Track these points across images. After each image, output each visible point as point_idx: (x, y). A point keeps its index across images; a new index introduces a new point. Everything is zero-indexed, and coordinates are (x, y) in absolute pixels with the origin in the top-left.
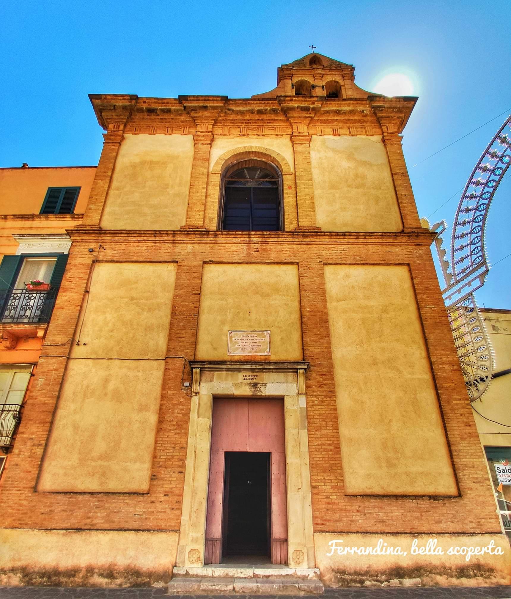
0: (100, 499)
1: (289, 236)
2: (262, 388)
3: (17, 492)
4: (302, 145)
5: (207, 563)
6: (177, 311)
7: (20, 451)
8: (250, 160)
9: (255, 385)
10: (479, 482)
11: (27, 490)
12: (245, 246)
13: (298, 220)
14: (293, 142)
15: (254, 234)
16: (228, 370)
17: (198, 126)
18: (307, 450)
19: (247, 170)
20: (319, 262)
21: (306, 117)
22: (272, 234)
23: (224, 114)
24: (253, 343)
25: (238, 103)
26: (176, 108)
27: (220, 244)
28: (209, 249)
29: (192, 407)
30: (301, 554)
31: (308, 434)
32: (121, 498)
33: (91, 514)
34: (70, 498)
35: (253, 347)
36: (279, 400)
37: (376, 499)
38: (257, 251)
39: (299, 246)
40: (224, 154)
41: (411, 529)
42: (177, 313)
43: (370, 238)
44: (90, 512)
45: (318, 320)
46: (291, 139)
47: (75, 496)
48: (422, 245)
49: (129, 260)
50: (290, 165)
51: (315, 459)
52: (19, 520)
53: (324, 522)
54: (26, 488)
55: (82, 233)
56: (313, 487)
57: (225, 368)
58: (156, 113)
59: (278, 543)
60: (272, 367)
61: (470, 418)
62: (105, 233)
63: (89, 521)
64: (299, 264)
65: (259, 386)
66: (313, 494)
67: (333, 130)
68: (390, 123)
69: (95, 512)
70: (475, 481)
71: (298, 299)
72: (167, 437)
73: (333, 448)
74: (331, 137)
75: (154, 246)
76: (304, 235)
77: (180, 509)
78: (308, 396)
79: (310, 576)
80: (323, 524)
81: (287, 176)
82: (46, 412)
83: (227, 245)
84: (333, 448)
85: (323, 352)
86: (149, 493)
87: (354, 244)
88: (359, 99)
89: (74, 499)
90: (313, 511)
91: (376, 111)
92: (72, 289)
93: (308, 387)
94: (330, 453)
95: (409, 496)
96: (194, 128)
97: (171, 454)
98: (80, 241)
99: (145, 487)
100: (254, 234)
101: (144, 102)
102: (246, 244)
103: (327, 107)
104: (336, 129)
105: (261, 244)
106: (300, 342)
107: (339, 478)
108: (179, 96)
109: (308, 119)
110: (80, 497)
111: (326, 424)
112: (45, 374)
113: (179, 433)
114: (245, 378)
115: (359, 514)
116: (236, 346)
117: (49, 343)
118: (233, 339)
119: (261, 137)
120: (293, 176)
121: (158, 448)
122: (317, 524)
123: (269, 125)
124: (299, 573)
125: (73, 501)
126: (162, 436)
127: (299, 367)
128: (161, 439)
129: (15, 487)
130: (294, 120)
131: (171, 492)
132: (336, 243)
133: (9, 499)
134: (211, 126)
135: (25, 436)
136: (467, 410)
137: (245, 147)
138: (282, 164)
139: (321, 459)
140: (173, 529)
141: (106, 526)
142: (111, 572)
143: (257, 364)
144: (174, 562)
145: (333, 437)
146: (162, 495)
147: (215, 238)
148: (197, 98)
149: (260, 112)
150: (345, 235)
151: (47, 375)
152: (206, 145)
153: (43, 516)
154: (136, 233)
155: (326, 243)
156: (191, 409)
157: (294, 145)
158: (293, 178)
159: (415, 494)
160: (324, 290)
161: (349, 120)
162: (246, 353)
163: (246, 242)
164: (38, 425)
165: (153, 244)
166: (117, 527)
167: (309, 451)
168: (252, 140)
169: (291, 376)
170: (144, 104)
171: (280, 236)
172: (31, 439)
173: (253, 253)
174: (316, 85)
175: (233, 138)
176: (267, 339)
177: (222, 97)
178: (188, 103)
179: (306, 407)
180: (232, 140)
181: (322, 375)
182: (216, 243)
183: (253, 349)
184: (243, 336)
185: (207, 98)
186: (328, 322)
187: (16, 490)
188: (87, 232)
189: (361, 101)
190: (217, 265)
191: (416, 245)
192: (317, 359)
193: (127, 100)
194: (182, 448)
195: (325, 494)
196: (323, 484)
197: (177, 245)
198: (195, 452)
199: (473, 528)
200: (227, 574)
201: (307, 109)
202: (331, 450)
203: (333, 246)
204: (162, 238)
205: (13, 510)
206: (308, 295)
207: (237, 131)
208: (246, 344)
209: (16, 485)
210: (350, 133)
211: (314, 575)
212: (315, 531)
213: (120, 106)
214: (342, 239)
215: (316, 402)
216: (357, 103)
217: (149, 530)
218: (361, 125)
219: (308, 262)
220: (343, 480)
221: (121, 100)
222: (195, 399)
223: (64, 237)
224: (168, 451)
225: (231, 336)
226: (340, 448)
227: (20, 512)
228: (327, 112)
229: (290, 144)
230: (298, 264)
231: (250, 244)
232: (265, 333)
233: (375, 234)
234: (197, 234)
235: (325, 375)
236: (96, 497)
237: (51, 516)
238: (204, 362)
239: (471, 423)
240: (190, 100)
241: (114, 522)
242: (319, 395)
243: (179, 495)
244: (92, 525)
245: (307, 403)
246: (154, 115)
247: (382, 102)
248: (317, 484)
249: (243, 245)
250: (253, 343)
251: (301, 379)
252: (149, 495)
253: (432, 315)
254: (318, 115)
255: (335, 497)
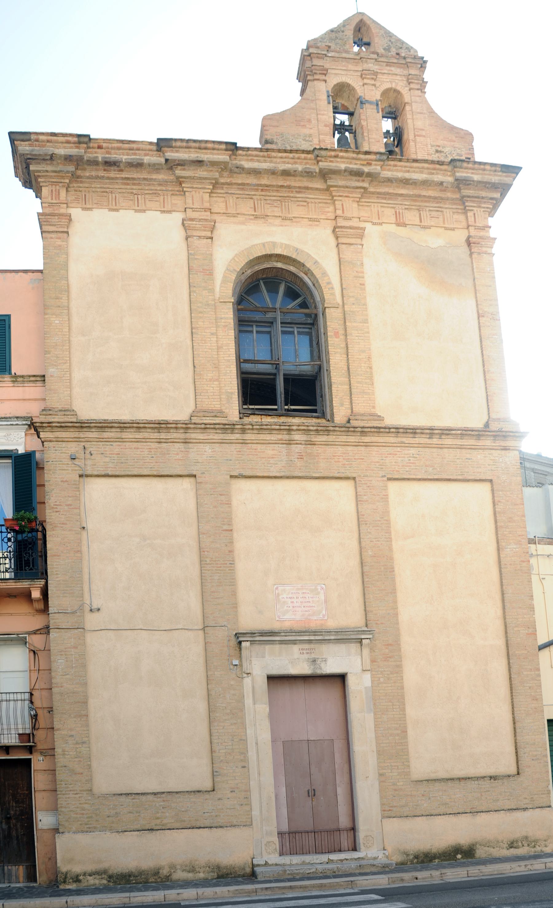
0: (165, 799)
1: (343, 433)
2: (323, 665)
3: (74, 796)
4: (352, 247)
5: (281, 854)
6: (207, 557)
7: (64, 751)
8: (271, 268)
9: (314, 661)
10: (538, 759)
11: (85, 793)
12: (283, 447)
13: (351, 399)
14: (337, 238)
15: (297, 430)
16: (282, 642)
17: (186, 193)
18: (373, 735)
19: (264, 283)
20: (382, 477)
21: (357, 188)
22: (321, 430)
23: (228, 173)
24: (305, 602)
25: (252, 156)
26: (152, 158)
27: (250, 445)
28: (235, 453)
29: (245, 691)
30: (371, 839)
31: (375, 718)
32: (186, 796)
33: (159, 815)
34: (133, 799)
35: (307, 609)
36: (342, 678)
37: (440, 783)
38: (301, 457)
39: (356, 448)
40: (233, 259)
41: (472, 808)
42: (208, 560)
43: (447, 437)
44: (158, 813)
45: (382, 568)
46: (334, 231)
47: (137, 797)
48: (509, 449)
49: (130, 473)
50: (335, 286)
51: (382, 745)
52: (86, 824)
53: (391, 809)
54: (84, 791)
55: (57, 427)
56: (381, 775)
57: (279, 641)
58: (118, 166)
59: (346, 832)
60: (333, 638)
61: (538, 691)
62: (89, 427)
63: (158, 822)
64: (357, 479)
65: (318, 662)
66: (380, 782)
67: (396, 212)
68: (480, 207)
69: (162, 812)
70: (534, 758)
71: (356, 535)
72: (223, 728)
73: (400, 732)
74: (393, 228)
75: (159, 448)
76: (362, 431)
77: (250, 804)
78: (373, 673)
79: (380, 857)
80: (390, 810)
81: (332, 309)
82: (79, 702)
83: (259, 446)
84: (400, 732)
85: (389, 614)
86: (214, 790)
87: (426, 446)
88: (438, 161)
89: (138, 801)
90: (381, 798)
91: (461, 186)
92: (63, 524)
93: (373, 661)
94: (397, 738)
95: (472, 778)
96: (180, 198)
97: (230, 747)
98: (54, 439)
99: (208, 785)
100: (297, 430)
101: (100, 147)
102: (285, 445)
103: (389, 170)
104: (401, 211)
105: (305, 444)
106: (361, 600)
107: (406, 763)
108: (158, 139)
109: (358, 190)
110: (143, 798)
111: (393, 705)
112: (63, 653)
113: (235, 724)
114: (302, 651)
115: (424, 798)
116: (286, 608)
117: (55, 609)
118: (281, 597)
119: (288, 222)
120: (340, 310)
121: (215, 741)
122: (384, 811)
123: (298, 195)
124: (369, 856)
125: (136, 802)
126: (218, 728)
127: (363, 637)
128: (216, 731)
129: (70, 791)
130: (338, 191)
131: (237, 788)
132: (403, 445)
133: (68, 804)
134: (208, 194)
135: (63, 733)
136: (536, 682)
137: (264, 244)
138: (323, 283)
139: (388, 745)
140: (245, 824)
141: (178, 825)
142: (193, 867)
143: (316, 634)
144: (252, 854)
145: (400, 720)
146: (228, 792)
147: (242, 435)
148: (188, 143)
149: (286, 173)
150: (415, 433)
151: (65, 655)
152: (205, 240)
153: (110, 819)
154: (133, 427)
155: (391, 445)
156: (245, 694)
157: (340, 245)
158: (341, 315)
159: (477, 775)
160: (388, 521)
161: (419, 196)
162: (298, 617)
163: (285, 442)
164: (75, 719)
165: (157, 445)
166: (189, 826)
167: (376, 737)
168: (274, 229)
169: (354, 647)
170: (99, 150)
171: (331, 433)
172: (72, 736)
173: (296, 460)
174: (367, 98)
175: (243, 223)
176: (322, 597)
177: (227, 143)
178: (172, 151)
179: (372, 686)
180: (243, 227)
181: (388, 645)
182: (244, 442)
183: (306, 611)
184: (292, 593)
185: (203, 145)
186: (394, 571)
187: (73, 794)
188: (63, 425)
189: (441, 165)
190: (248, 480)
191: (502, 450)
192: (382, 623)
193: (74, 143)
194: (241, 740)
195: (392, 781)
196: (390, 771)
197: (190, 445)
198: (257, 744)
199: (527, 804)
200: (304, 861)
201: (358, 174)
202: (398, 735)
203: (399, 449)
204: (169, 434)
205: (77, 814)
206: (369, 530)
207: (246, 207)
208: (298, 605)
209: (72, 789)
210: (421, 221)
211: (383, 856)
212: (383, 817)
213: (61, 156)
214: (411, 439)
215: (382, 680)
216: (434, 169)
217: (221, 827)
218: (437, 205)
219: (367, 476)
220: (409, 766)
221: (62, 143)
222: (247, 681)
223: (14, 423)
224: (226, 744)
225: (278, 594)
226: (407, 732)
227: (85, 816)
228: (389, 180)
229: (332, 241)
230: (354, 479)
231: (290, 444)
232: (319, 588)
233: (454, 432)
234: (218, 428)
235: (391, 645)
236: (160, 798)
237: (119, 818)
238: (254, 633)
239: (538, 697)
240: (176, 147)
241: (184, 821)
242: (385, 671)
243: (246, 791)
244: (163, 825)
245: (372, 682)
246: (115, 170)
247: (470, 171)
248: (384, 771)
249: (280, 445)
250: (305, 602)
251: (366, 651)
252: (215, 792)
253: (513, 558)
254: (375, 183)
255: (402, 783)
